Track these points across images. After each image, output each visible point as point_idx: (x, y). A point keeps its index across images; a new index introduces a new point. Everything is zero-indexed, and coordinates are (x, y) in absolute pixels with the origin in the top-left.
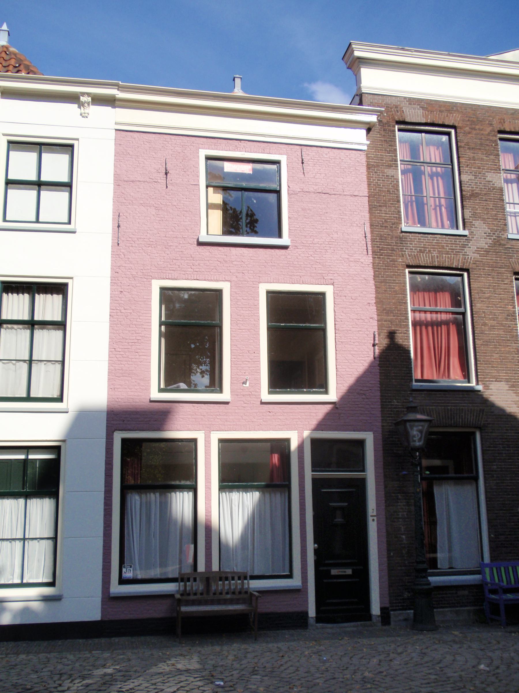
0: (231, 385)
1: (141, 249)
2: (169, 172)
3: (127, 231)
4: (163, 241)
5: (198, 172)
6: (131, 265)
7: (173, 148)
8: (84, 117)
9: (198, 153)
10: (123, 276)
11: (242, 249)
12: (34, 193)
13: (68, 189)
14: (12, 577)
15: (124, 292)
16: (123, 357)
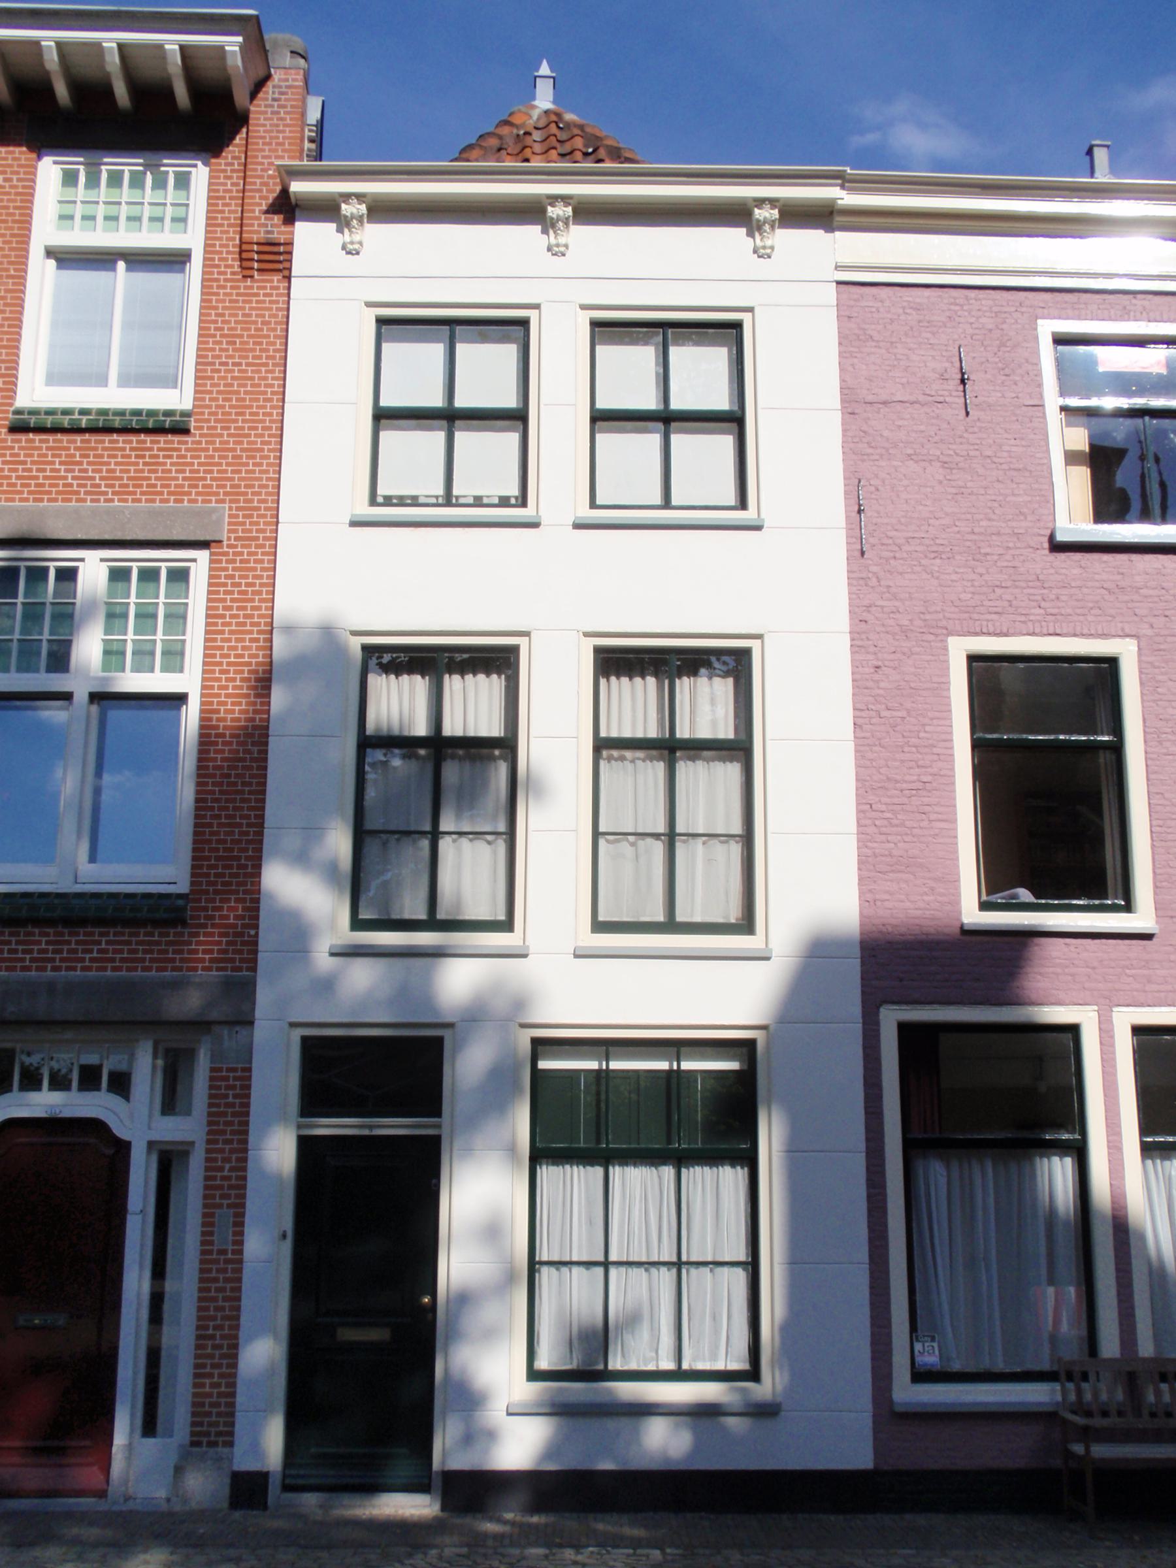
0: (1155, 894)
1: (916, 563)
2: (972, 377)
3: (879, 520)
4: (968, 544)
5: (1039, 374)
6: (897, 604)
7: (973, 320)
8: (349, 253)
9: (1036, 329)
10: (877, 629)
11: (1160, 557)
12: (440, 437)
13: (519, 424)
14: (654, 1354)
15: (884, 668)
16: (892, 825)
